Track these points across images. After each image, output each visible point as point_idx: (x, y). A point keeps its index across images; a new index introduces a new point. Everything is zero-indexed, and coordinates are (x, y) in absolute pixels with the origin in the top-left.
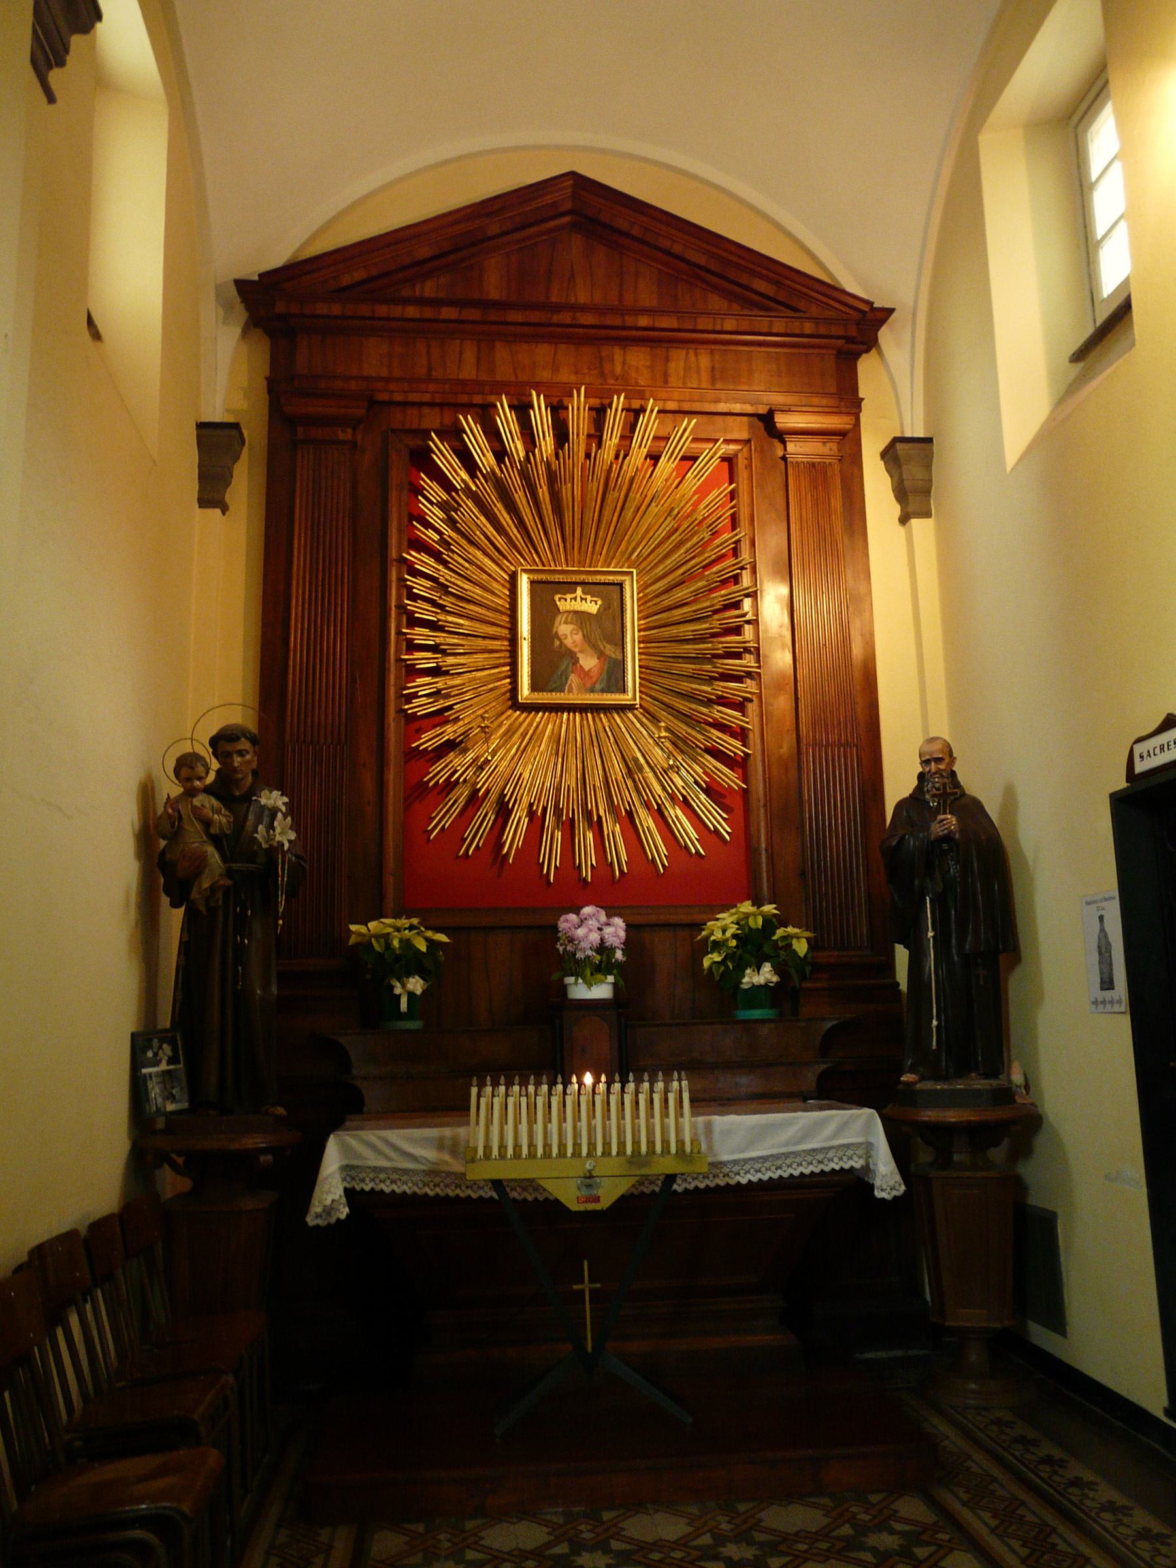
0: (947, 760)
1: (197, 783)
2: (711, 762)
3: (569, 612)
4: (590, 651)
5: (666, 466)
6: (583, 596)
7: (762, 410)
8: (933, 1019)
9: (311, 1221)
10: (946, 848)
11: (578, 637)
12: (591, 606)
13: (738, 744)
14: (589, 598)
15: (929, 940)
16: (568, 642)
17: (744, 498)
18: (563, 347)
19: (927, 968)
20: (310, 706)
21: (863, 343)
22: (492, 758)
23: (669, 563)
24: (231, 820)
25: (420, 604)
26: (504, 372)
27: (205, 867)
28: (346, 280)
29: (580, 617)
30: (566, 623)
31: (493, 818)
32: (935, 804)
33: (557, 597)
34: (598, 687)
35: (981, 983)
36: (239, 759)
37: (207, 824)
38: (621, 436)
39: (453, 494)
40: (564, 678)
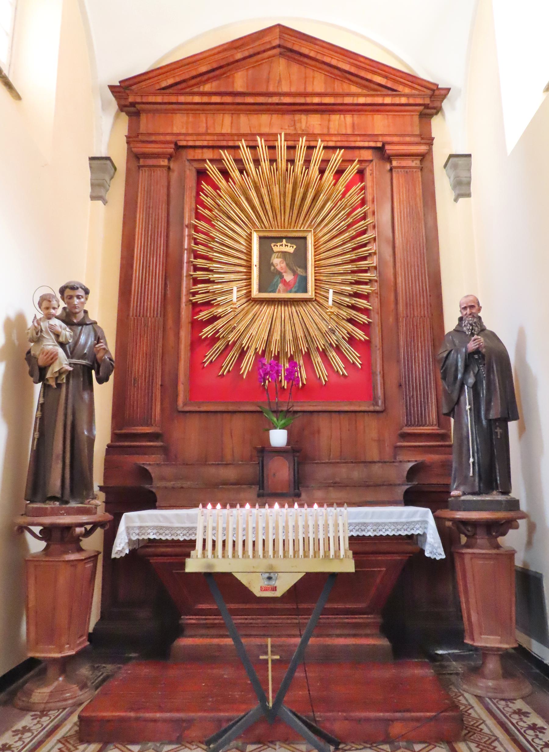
0: (477, 307)
1: (52, 311)
2: (350, 326)
3: (279, 252)
4: (289, 271)
5: (329, 176)
6: (287, 244)
7: (379, 145)
8: (470, 458)
9: (113, 556)
10: (477, 357)
11: (284, 265)
12: (290, 249)
13: (365, 317)
14: (289, 245)
15: (467, 411)
16: (278, 267)
17: (369, 190)
18: (274, 116)
19: (465, 429)
20: (143, 295)
21: (434, 108)
22: (238, 326)
23: (331, 226)
24: (72, 334)
25: (200, 246)
26: (244, 129)
27: (56, 359)
28: (164, 84)
29: (284, 254)
30: (277, 258)
31: (237, 356)
32: (470, 333)
33: (272, 245)
34: (293, 290)
35: (499, 437)
36: (78, 300)
37: (57, 335)
38: (305, 160)
39: (218, 191)
40: (276, 286)
